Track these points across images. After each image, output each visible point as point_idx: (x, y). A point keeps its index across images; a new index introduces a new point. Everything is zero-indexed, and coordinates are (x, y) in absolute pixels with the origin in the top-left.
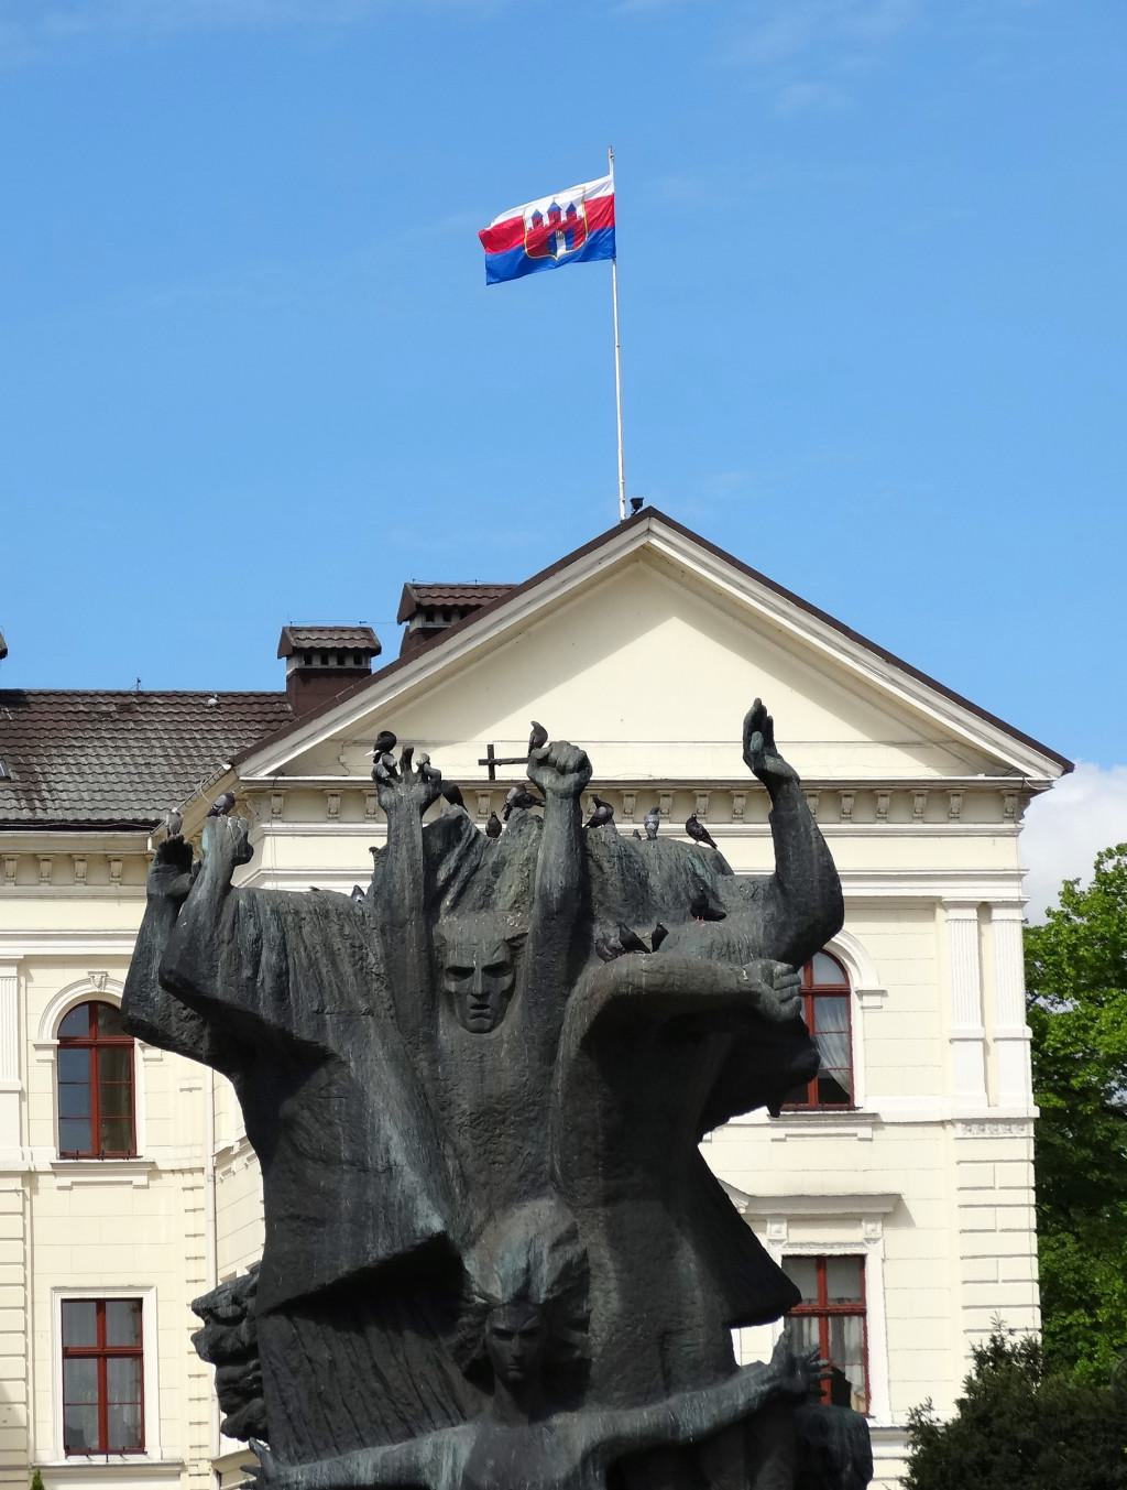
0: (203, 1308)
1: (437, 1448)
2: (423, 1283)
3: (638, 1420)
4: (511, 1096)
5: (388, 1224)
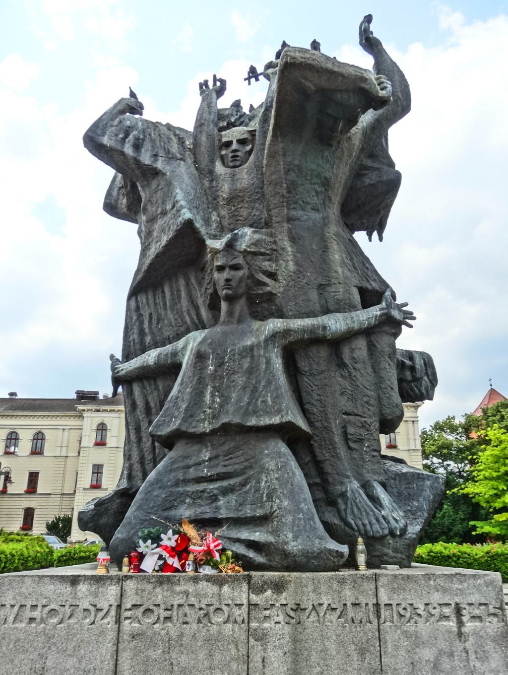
4: (247, 189)
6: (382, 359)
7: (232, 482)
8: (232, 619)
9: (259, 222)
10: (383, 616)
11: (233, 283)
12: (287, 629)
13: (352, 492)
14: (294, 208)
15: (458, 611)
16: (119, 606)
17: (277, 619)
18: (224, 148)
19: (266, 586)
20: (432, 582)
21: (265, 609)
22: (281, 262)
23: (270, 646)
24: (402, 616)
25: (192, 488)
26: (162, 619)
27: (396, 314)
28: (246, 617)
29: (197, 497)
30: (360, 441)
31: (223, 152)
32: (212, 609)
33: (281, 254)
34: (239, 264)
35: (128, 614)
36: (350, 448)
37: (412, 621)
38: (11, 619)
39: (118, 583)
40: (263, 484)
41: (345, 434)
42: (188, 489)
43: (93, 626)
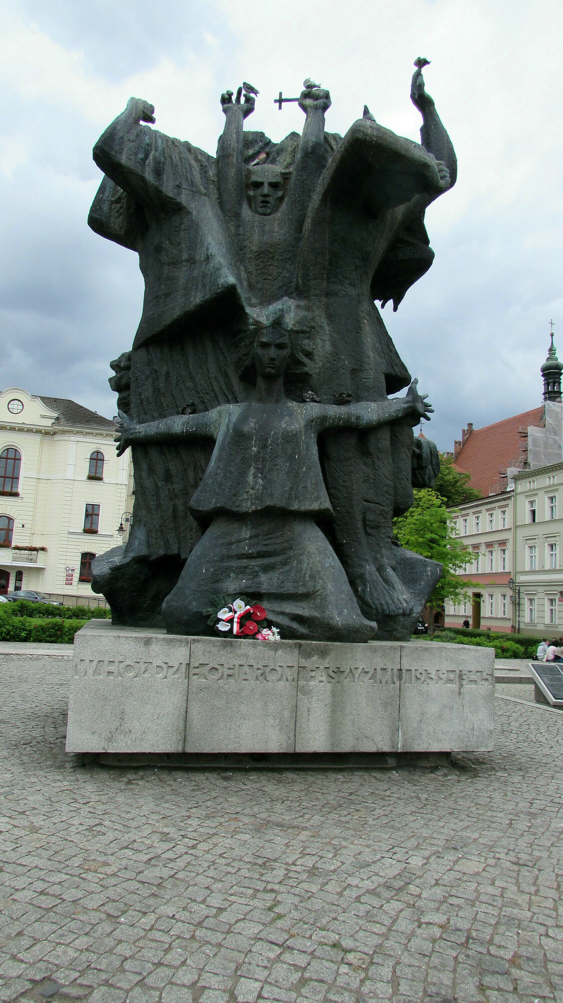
0: (115, 366)
1: (220, 413)
2: (220, 316)
3: (334, 411)
5: (204, 286)
6: (402, 450)
7: (272, 560)
8: (284, 678)
9: (290, 285)
10: (404, 678)
11: (277, 363)
12: (329, 686)
13: (371, 575)
14: (333, 282)
15: (461, 677)
16: (188, 665)
17: (321, 679)
18: (252, 188)
19: (313, 653)
20: (443, 654)
21: (312, 671)
22: (318, 341)
23: (314, 699)
24: (418, 679)
25: (234, 563)
26: (225, 676)
27: (420, 407)
28: (296, 676)
29: (242, 571)
30: (377, 527)
31: (251, 193)
32: (268, 669)
33: (318, 332)
34: (285, 344)
35: (197, 671)
36: (367, 534)
37: (425, 683)
38: (90, 672)
39: (187, 645)
40: (305, 565)
41: (364, 520)
42: (233, 564)
43: (166, 680)
